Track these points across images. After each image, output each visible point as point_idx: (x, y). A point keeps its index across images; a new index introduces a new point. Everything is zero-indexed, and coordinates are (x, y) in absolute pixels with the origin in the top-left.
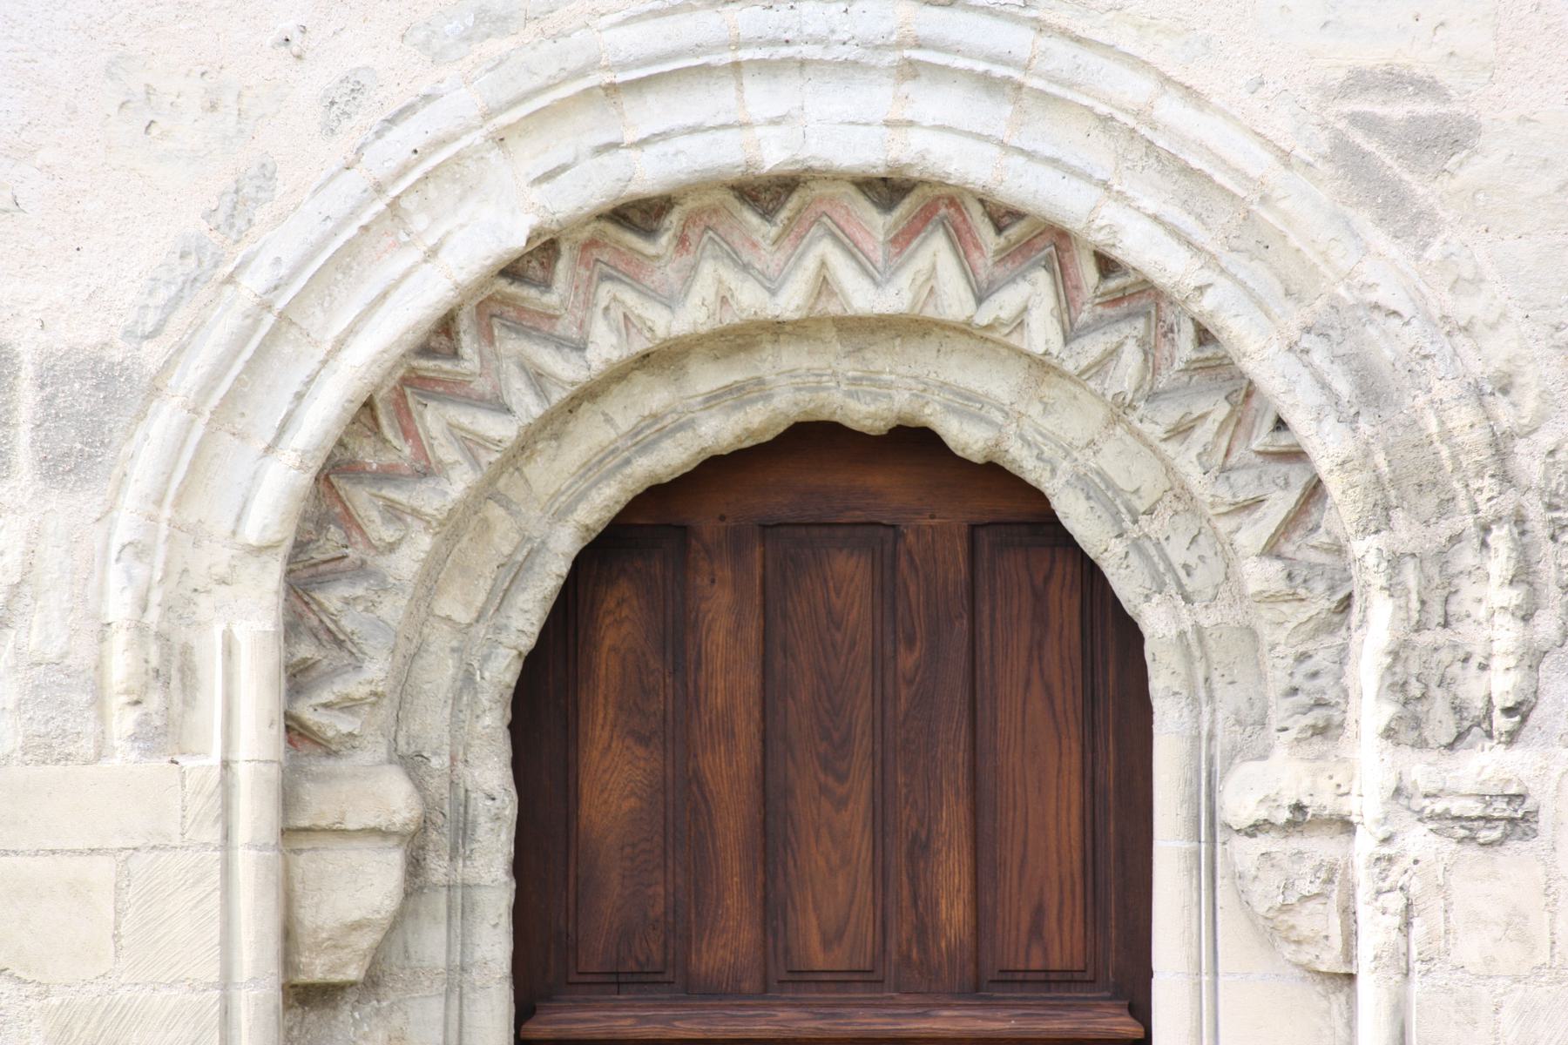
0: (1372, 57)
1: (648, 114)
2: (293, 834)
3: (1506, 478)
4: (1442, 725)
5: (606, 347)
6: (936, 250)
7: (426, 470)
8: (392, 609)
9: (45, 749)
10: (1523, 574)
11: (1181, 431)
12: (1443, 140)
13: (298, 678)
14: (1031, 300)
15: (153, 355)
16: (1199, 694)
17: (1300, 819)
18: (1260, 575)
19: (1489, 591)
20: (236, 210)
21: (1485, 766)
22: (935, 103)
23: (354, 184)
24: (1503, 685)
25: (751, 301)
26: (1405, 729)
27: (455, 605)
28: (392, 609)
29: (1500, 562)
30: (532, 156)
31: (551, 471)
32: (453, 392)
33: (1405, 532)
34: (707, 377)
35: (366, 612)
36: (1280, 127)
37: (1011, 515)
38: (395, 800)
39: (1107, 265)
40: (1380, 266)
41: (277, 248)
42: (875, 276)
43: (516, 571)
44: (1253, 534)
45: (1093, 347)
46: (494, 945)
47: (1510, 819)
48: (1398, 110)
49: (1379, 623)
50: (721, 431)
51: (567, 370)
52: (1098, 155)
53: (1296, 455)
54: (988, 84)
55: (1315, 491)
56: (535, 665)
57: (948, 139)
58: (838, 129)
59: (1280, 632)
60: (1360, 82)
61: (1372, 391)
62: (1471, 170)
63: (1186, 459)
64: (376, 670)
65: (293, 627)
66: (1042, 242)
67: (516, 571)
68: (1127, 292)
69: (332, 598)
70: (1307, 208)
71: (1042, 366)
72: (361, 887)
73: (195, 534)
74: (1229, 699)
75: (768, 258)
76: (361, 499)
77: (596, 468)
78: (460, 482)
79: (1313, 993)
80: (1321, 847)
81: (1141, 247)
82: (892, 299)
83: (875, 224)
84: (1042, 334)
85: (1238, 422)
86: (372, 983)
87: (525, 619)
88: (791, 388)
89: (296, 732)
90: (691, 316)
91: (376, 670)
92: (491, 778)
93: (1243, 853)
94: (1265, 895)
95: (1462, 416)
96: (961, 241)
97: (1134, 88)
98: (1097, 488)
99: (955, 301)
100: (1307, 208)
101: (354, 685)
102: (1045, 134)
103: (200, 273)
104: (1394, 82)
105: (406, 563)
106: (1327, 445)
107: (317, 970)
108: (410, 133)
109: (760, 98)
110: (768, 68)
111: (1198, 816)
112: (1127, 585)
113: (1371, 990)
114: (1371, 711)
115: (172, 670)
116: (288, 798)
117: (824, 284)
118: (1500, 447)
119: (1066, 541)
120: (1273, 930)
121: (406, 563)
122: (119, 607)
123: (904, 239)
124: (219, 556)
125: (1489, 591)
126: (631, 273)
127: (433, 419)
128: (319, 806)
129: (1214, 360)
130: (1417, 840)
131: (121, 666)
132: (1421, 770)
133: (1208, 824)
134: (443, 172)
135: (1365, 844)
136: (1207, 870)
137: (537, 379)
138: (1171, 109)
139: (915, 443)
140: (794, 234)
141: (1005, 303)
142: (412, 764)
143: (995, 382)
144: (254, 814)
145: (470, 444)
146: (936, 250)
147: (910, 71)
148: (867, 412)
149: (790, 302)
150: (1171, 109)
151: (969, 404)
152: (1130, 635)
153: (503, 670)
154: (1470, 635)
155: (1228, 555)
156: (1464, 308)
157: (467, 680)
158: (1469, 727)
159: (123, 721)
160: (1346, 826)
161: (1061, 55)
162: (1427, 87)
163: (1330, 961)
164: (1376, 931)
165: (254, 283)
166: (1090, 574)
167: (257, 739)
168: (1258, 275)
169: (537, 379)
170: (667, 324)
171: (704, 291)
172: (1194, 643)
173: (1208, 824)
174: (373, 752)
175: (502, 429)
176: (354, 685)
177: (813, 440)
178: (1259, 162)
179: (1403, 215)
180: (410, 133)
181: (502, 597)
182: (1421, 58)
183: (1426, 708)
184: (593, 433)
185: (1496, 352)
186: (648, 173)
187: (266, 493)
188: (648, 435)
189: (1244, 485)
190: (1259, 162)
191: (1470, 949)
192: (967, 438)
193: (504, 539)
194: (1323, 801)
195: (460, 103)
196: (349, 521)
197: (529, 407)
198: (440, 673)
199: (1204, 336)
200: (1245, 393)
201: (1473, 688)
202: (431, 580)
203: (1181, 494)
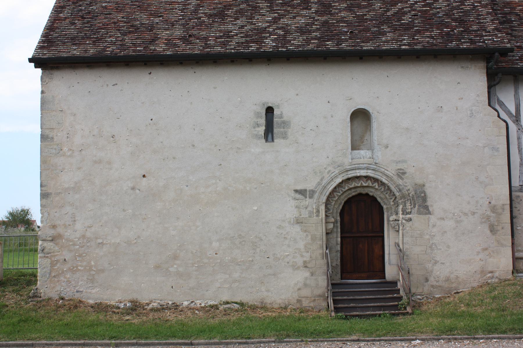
0: (399, 168)
1: (350, 172)
2: (326, 222)
3: (409, 196)
4: (405, 213)
5: (347, 188)
6: (369, 181)
7: (334, 197)
8: (332, 207)
9: (310, 217)
10: (411, 203)
11: (387, 193)
12: (404, 173)
13: (326, 212)
14: (376, 185)
15: (316, 190)
16: (388, 212)
17: (396, 220)
18: (392, 203)
19: (408, 204)
20: (322, 180)
21: (408, 216)
22: (369, 171)
23: (330, 178)
24: (409, 210)
25: (356, 185)
26: (403, 214)
27: (336, 206)
28: (332, 207)
29: (409, 202)
30: (342, 175)
31: (342, 197)
32: (336, 192)
33: (403, 200)
34: (353, 190)
35: (331, 207)
36: (393, 172)
37: (374, 199)
38: (333, 220)
39: (381, 182)
40: (400, 182)
41: (324, 182)
42: (365, 183)
43: (340, 204)
44: (392, 201)
45: (380, 188)
46: (339, 230)
47: (410, 220)
48: (401, 171)
49: (401, 207)
50: (354, 194)
51: (344, 190)
52: (381, 174)
53: (395, 195)
54: (373, 170)
55: (396, 197)
56: (341, 210)
57: (370, 173)
58: (363, 173)
59: (393, 208)
60: (398, 169)
61: (400, 190)
62: (406, 175)
63: (387, 196)
64: (331, 211)
65: (326, 208)
66: (376, 180)
67: (340, 204)
68: (383, 184)
69: (328, 206)
70: (395, 178)
71: (376, 189)
72: (331, 226)
73: (319, 202)
74: (390, 212)
75: (358, 182)
76: (330, 199)
77: (345, 197)
78: (337, 198)
79: (396, 232)
80: (397, 222)
81: (384, 180)
82: (366, 185)
83: (365, 179)
84: (377, 187)
85: (390, 193)
86: (331, 233)
87: (341, 207)
88: (359, 191)
89: (326, 216)
90: (352, 186)
91: (331, 211)
92: (339, 218)
93: (392, 222)
94: (393, 225)
95: (406, 192)
96: (371, 181)
97: (383, 170)
98: (380, 198)
99: (371, 185)
100: (395, 178)
101: (330, 212)
102: (377, 173)
103: (319, 184)
104: (401, 169)
105: (333, 204)
106: (397, 194)
107: (328, 232)
108: (334, 174)
109: (357, 171)
110: (358, 169)
111: (378, 306)
112: (382, 204)
113: (401, 232)
114: (401, 212)
115: (318, 211)
116: (326, 220)
117: (362, 184)
118: (409, 194)
119: (378, 201)
120: (394, 228)
121: (333, 204)
122: (314, 207)
123: (367, 181)
124: (321, 203)
125: (408, 204)
126: (348, 183)
127: (335, 194)
128: (328, 220)
129: (389, 189)
130: (404, 221)
131: (315, 211)
132: (404, 216)
133: (388, 221)
134: (336, 177)
135: (400, 222)
136: (388, 224)
137: (342, 191)
138: (386, 171)
139: (367, 194)
140: (359, 180)
141: (374, 185)
142: (333, 217)
143: (373, 190)
144: (324, 221)
145: (337, 195)
146: (369, 181)
147: (368, 169)
148: (364, 192)
149: (359, 185)
150: (386, 171)
151: (371, 192)
152: (382, 208)
153: (339, 211)
154: (407, 207)
155: (390, 202)
156: (406, 185)
157: (337, 212)
158: (408, 213)
159: (315, 215)
160: (399, 220)
161: (378, 168)
162: (403, 170)
163: (397, 230)
164: (401, 228)
165: (323, 184)
166: (379, 204)
167: (324, 216)
168: (392, 183)
169: (342, 191)
170: (351, 187)
171: (353, 185)
172: (387, 208)
173: (388, 221)
174: (331, 217)
175: (339, 194)
176: (330, 212)
177: (360, 194)
178: (392, 175)
179: (402, 179)
180: (334, 174)
181: (339, 206)
182: (402, 168)
183: (404, 212)
184: (345, 194)
185: (409, 187)
186: (350, 176)
187: (324, 199)
188: (349, 194)
189: (391, 197)
190: (392, 175)
191: (407, 229)
192: (371, 194)
193: (339, 202)
194: (397, 219)
195: (337, 172)
196: (329, 201)
197: (341, 193)
198: (335, 211)
199: (388, 187)
200: (391, 191)
201: (407, 211)
202: (334, 205)
203: (386, 198)
